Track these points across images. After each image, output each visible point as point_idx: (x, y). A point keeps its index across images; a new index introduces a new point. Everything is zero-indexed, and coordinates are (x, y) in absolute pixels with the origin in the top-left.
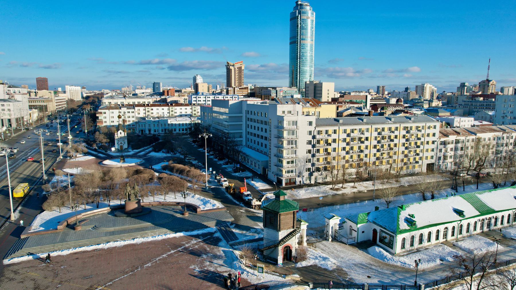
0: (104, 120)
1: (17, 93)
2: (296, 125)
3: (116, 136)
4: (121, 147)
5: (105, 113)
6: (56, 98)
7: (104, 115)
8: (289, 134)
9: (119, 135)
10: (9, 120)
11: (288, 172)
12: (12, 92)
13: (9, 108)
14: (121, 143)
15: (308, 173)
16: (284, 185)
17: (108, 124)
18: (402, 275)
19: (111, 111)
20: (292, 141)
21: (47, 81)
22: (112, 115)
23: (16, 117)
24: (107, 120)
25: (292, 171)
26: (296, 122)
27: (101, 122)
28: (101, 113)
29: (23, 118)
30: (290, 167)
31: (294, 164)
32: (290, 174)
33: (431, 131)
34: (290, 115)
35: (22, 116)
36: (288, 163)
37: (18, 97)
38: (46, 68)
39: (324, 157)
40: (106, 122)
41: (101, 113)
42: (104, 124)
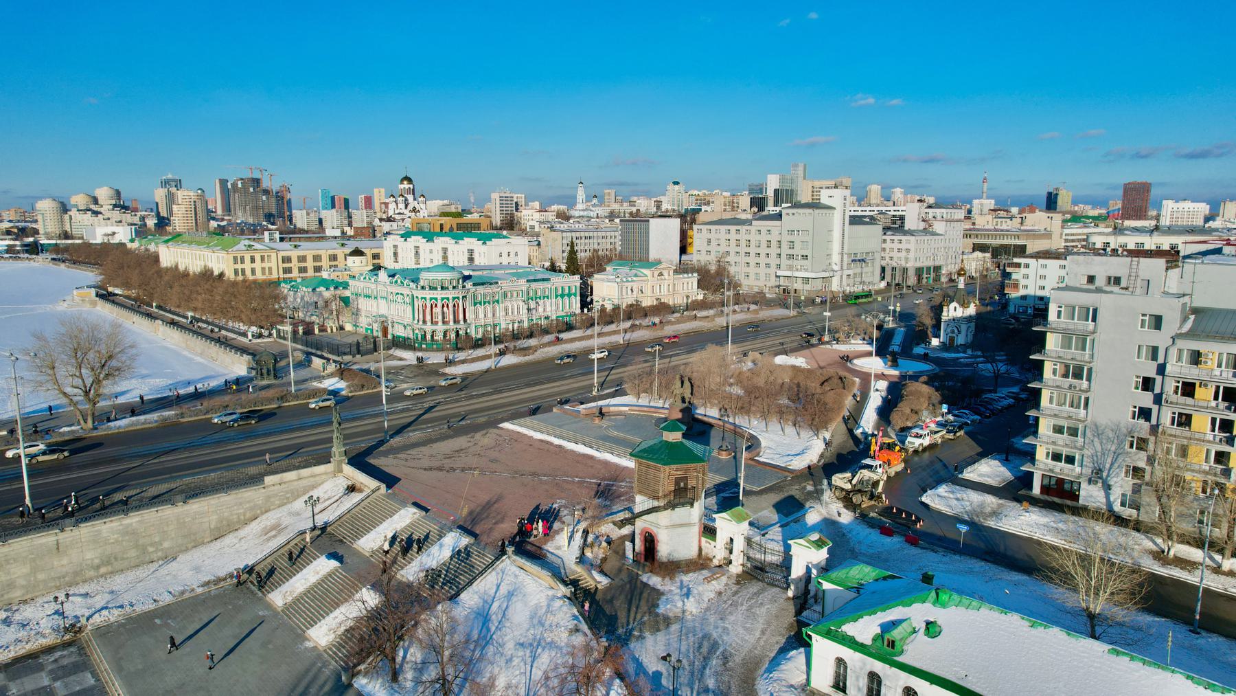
0: (1022, 282)
1: (939, 217)
2: (1094, 320)
3: (945, 313)
4: (952, 339)
5: (1027, 266)
6: (1066, 231)
7: (1023, 270)
8: (1067, 344)
9: (952, 314)
10: (894, 269)
11: (1057, 457)
12: (931, 216)
13: (908, 246)
14: (953, 332)
15: (1130, 481)
16: (1036, 490)
17: (1030, 291)
18: (63, 434)
19: (1041, 261)
20: (1081, 369)
21: (1148, 191)
22: (1042, 272)
23: (919, 265)
24: (1030, 283)
25: (1070, 460)
26: (1095, 311)
27: (1015, 286)
28: (1018, 265)
29: (937, 269)
30: (1063, 443)
31: (1080, 439)
32: (1063, 464)
33: (548, 309)
34: (1116, 289)
35: (937, 264)
36: (1058, 430)
37: (939, 227)
38: (1193, 156)
39: (1214, 449)
40: (1026, 287)
41: (1018, 265)
42: (1022, 292)
